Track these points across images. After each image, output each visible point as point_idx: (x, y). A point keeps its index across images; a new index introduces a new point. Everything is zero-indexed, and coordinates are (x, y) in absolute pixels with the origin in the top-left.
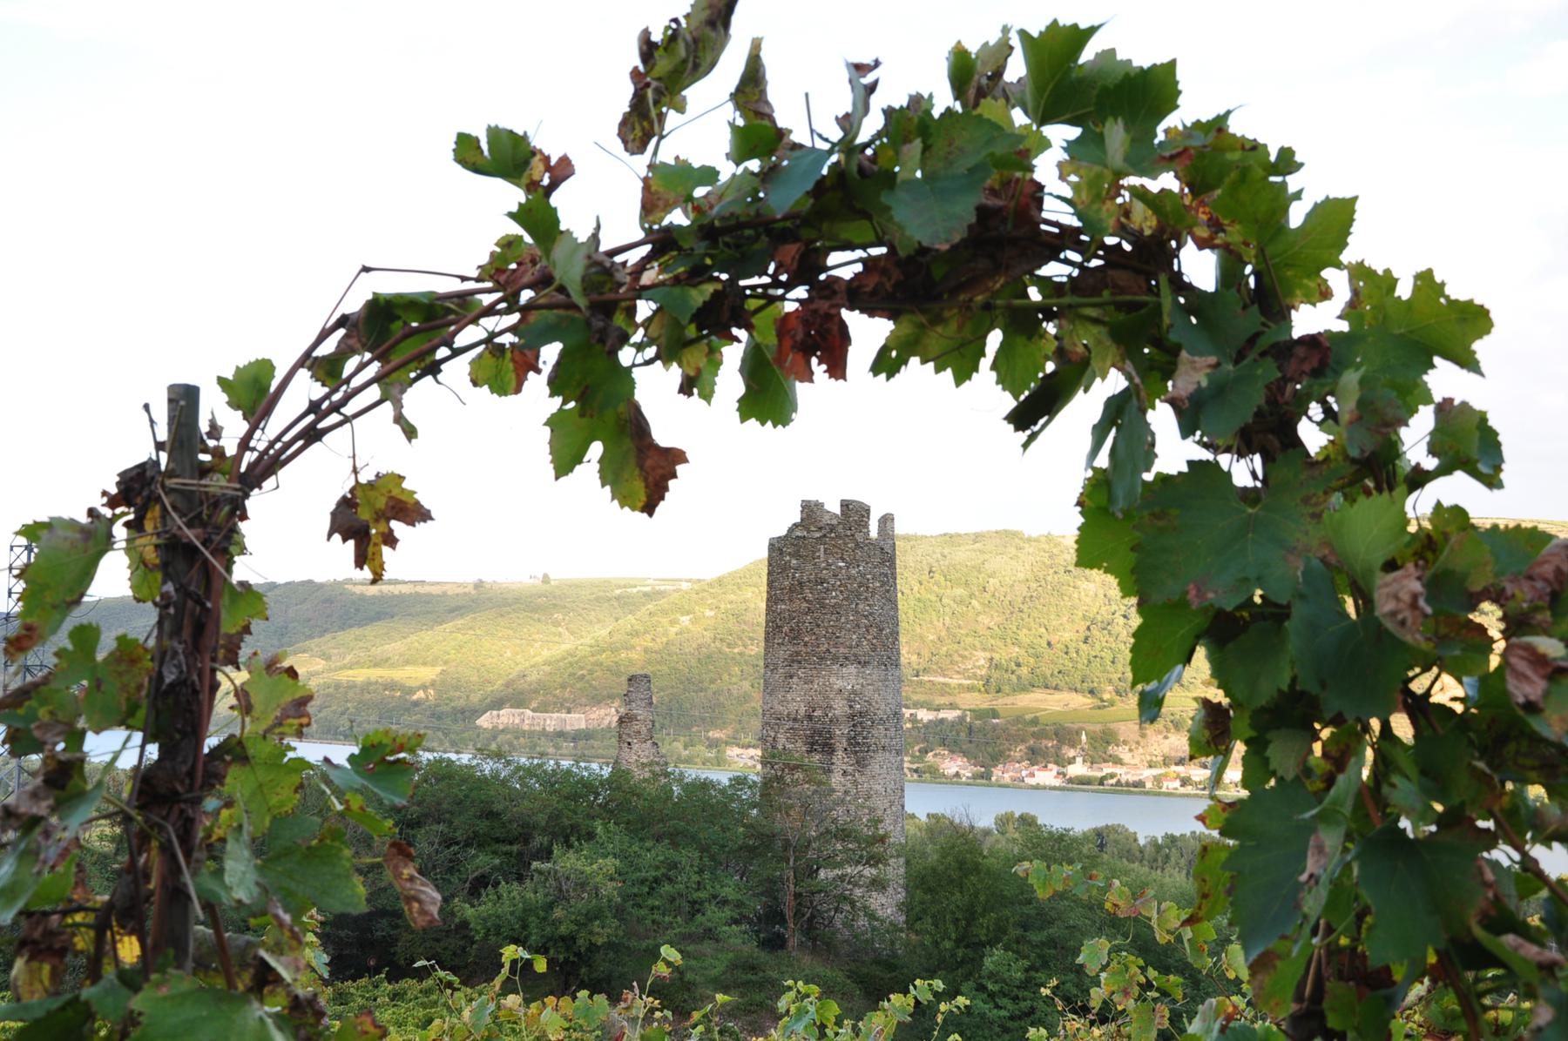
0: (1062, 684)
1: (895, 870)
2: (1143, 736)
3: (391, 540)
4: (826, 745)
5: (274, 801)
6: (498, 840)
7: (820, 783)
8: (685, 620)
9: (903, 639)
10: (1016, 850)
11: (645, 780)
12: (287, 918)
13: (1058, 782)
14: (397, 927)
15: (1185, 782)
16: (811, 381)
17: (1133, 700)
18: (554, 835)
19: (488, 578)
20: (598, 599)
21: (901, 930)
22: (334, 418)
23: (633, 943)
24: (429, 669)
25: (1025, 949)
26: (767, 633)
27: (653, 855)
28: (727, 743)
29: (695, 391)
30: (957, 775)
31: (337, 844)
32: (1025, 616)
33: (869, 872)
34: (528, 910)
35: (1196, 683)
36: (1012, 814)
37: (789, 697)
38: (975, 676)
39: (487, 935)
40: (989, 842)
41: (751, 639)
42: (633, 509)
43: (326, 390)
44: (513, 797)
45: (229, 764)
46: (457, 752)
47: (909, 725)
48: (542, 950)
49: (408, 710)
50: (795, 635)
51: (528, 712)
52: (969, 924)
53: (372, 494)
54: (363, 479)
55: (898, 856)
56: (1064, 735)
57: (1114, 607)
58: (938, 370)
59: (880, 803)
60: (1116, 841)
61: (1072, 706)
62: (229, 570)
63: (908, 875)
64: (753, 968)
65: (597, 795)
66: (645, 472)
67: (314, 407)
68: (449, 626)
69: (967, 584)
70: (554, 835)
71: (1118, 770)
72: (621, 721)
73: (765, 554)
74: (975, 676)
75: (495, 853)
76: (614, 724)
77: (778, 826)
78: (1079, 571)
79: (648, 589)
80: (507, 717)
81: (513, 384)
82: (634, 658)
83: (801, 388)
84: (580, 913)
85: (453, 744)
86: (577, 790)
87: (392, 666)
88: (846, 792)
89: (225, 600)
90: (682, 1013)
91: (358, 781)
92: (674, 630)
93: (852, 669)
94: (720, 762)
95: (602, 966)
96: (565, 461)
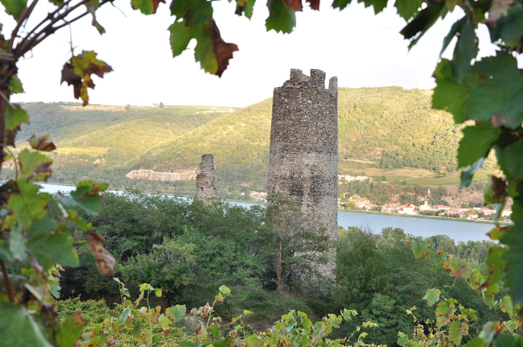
0: (419, 165)
1: (332, 254)
2: (460, 192)
3: (91, 85)
4: (299, 191)
5: (33, 213)
6: (136, 234)
7: (296, 210)
8: (231, 128)
9: (339, 140)
10: (392, 246)
11: (209, 206)
12: (40, 268)
13: (415, 213)
14: (86, 274)
15: (481, 215)
16: (301, 10)
17: (457, 174)
18: (164, 232)
19: (132, 104)
20: (187, 116)
21: (333, 283)
22: (60, 22)
23: (202, 285)
24: (103, 149)
25: (395, 294)
26: (272, 135)
27: (212, 243)
28: (250, 189)
29: (243, 13)
30: (364, 208)
31: (64, 233)
32: (402, 131)
33: (318, 254)
34: (150, 268)
35: (490, 167)
36: (391, 228)
37: (282, 167)
38: (375, 160)
39: (130, 279)
40: (379, 241)
41: (264, 138)
42: (211, 73)
43: (56, 7)
44: (144, 213)
45: (9, 194)
46: (116, 190)
47: (341, 183)
48: (157, 286)
49: (92, 168)
50: (286, 137)
51: (152, 171)
52: (367, 281)
53: (81, 62)
54: (76, 54)
55: (333, 247)
56: (420, 191)
57: (448, 127)
58: (367, 6)
59: (325, 221)
60: (444, 244)
61: (424, 176)
62: (8, 98)
63: (338, 257)
64: (260, 299)
65: (186, 213)
66: (217, 55)
67: (50, 16)
68: (112, 127)
69: (373, 113)
70: (164, 232)
71: (446, 208)
72: (198, 177)
73: (271, 96)
74: (375, 160)
75: (135, 239)
76: (195, 178)
77: (274, 231)
78: (432, 111)
79: (213, 112)
80: (141, 173)
81: (152, 9)
82: (205, 147)
83: (298, 14)
84: (176, 270)
85: (115, 186)
86: (175, 210)
87: (84, 147)
88: (309, 215)
89: (7, 113)
90: (226, 319)
91: (75, 203)
92: (225, 133)
93: (314, 154)
94: (247, 198)
95: (186, 295)
96: (178, 48)
